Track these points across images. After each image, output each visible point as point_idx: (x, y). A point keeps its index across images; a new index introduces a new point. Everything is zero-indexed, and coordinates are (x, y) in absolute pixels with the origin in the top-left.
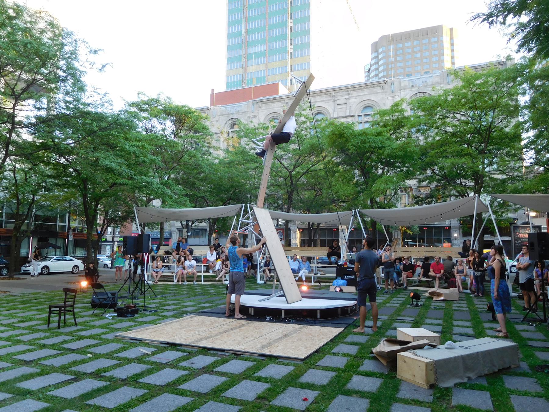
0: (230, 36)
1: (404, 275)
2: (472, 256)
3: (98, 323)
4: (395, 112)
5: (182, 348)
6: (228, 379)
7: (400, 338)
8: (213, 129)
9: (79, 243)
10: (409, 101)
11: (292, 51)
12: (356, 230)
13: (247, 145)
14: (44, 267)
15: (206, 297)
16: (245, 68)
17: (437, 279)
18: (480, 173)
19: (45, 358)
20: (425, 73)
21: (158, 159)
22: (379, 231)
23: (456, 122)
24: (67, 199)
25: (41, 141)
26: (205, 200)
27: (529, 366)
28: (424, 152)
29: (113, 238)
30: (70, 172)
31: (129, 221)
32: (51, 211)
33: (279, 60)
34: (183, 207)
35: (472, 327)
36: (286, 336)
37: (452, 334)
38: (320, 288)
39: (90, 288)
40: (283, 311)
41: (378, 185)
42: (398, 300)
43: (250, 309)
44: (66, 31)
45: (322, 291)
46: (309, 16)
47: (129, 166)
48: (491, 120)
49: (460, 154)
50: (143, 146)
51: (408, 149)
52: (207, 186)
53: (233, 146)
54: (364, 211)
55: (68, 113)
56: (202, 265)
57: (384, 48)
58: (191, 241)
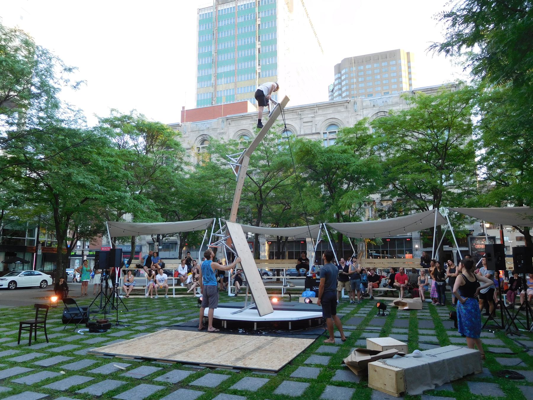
0: (200, 56)
1: (370, 285)
2: (433, 266)
3: (69, 339)
4: (359, 130)
5: (157, 362)
6: (204, 393)
7: (369, 347)
8: (184, 145)
9: (47, 257)
10: (371, 120)
11: (260, 71)
12: (324, 242)
13: (218, 160)
14: (11, 282)
15: (178, 310)
16: (215, 86)
17: (401, 289)
18: (438, 187)
19: (16, 376)
20: (384, 93)
21: (130, 173)
22: (344, 242)
23: (415, 141)
24: (37, 213)
25: (11, 156)
26: (177, 215)
27: (491, 372)
28: (386, 168)
29: (83, 252)
30: (41, 186)
31: (99, 235)
32: (20, 225)
33: (248, 80)
34: (155, 222)
35: (436, 336)
36: (259, 348)
37: (418, 342)
38: (290, 299)
39: (61, 303)
40: (255, 323)
41: (344, 200)
42: (365, 310)
43: (223, 322)
44: (40, 48)
45: (292, 302)
46: (276, 39)
47: (102, 183)
48: (447, 138)
49: (420, 170)
50: (116, 161)
51: (372, 166)
52: (177, 201)
53: (203, 162)
54: (332, 225)
55: (41, 129)
56: (174, 278)
57: (347, 70)
58: (162, 254)
